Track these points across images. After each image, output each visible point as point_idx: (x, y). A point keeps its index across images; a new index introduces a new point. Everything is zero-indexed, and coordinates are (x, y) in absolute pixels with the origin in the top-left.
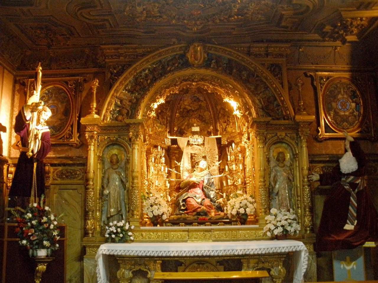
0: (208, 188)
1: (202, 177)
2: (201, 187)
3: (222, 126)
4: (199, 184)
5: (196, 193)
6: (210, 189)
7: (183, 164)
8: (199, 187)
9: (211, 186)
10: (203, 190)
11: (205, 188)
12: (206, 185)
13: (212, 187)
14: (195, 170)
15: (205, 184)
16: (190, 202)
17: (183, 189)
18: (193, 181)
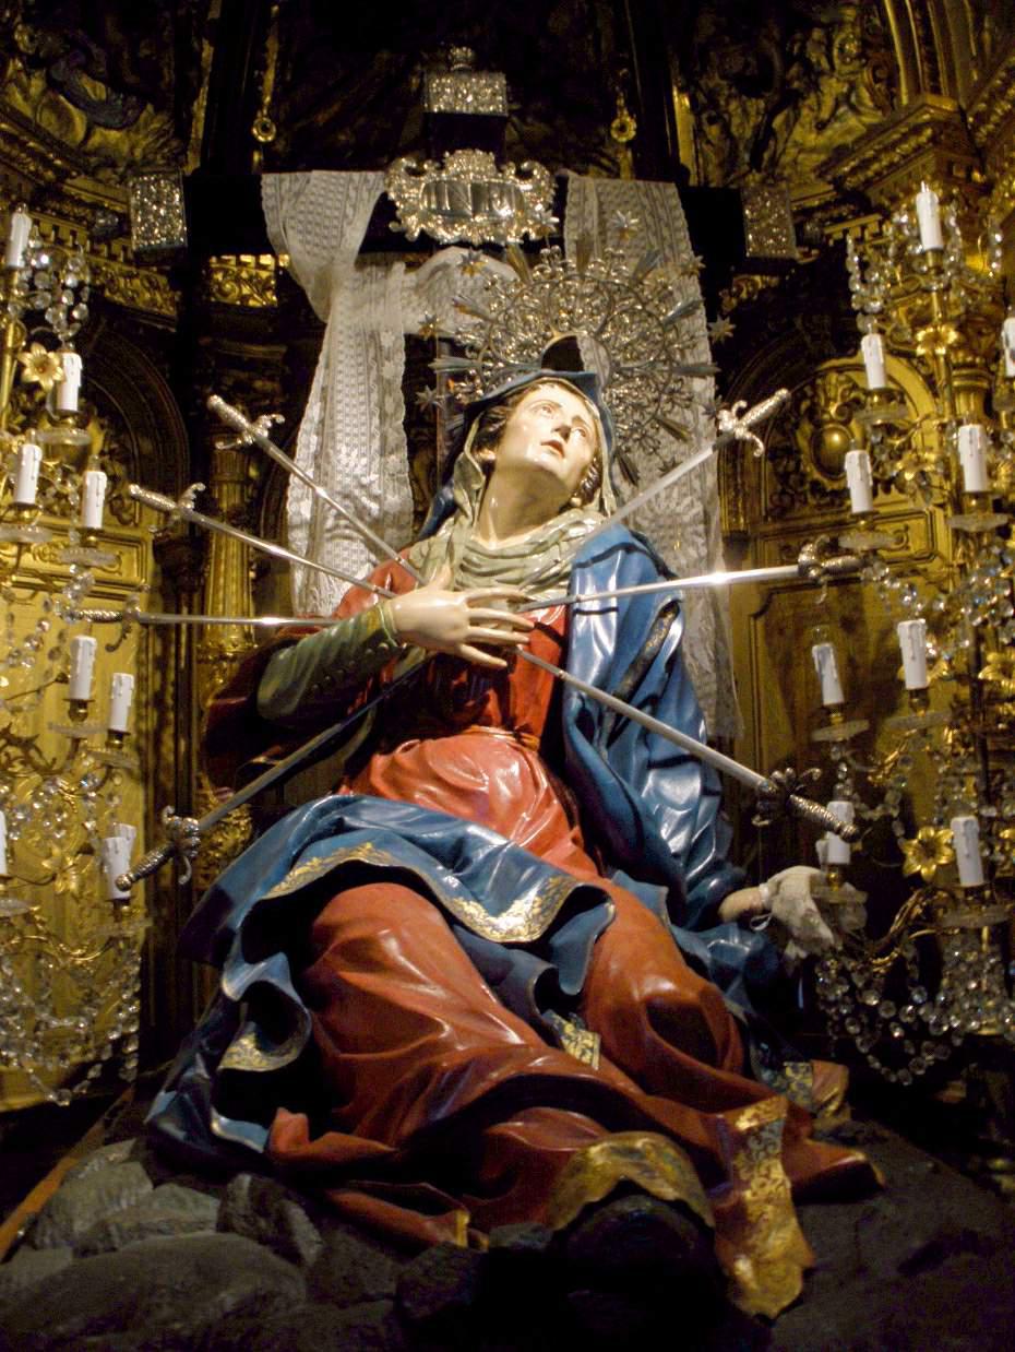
0: (622, 722)
1: (542, 583)
2: (533, 714)
3: (726, 129)
4: (499, 679)
5: (462, 793)
6: (646, 735)
7: (320, 457)
8: (508, 723)
9: (654, 703)
10: (555, 755)
11: (586, 722)
12: (603, 683)
13: (671, 710)
14: (452, 509)
15: (584, 675)
16: (364, 954)
17: (285, 732)
18: (418, 635)
